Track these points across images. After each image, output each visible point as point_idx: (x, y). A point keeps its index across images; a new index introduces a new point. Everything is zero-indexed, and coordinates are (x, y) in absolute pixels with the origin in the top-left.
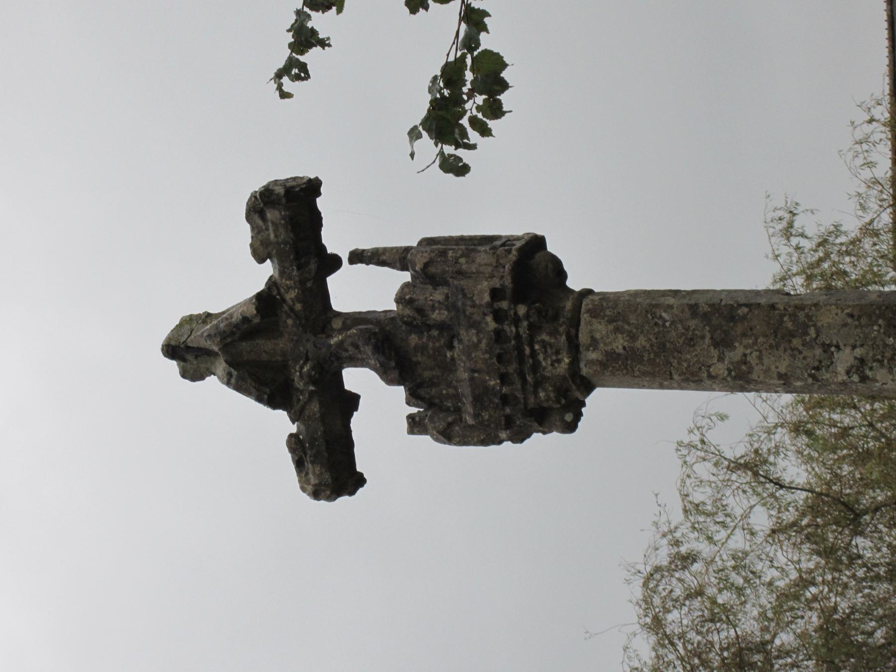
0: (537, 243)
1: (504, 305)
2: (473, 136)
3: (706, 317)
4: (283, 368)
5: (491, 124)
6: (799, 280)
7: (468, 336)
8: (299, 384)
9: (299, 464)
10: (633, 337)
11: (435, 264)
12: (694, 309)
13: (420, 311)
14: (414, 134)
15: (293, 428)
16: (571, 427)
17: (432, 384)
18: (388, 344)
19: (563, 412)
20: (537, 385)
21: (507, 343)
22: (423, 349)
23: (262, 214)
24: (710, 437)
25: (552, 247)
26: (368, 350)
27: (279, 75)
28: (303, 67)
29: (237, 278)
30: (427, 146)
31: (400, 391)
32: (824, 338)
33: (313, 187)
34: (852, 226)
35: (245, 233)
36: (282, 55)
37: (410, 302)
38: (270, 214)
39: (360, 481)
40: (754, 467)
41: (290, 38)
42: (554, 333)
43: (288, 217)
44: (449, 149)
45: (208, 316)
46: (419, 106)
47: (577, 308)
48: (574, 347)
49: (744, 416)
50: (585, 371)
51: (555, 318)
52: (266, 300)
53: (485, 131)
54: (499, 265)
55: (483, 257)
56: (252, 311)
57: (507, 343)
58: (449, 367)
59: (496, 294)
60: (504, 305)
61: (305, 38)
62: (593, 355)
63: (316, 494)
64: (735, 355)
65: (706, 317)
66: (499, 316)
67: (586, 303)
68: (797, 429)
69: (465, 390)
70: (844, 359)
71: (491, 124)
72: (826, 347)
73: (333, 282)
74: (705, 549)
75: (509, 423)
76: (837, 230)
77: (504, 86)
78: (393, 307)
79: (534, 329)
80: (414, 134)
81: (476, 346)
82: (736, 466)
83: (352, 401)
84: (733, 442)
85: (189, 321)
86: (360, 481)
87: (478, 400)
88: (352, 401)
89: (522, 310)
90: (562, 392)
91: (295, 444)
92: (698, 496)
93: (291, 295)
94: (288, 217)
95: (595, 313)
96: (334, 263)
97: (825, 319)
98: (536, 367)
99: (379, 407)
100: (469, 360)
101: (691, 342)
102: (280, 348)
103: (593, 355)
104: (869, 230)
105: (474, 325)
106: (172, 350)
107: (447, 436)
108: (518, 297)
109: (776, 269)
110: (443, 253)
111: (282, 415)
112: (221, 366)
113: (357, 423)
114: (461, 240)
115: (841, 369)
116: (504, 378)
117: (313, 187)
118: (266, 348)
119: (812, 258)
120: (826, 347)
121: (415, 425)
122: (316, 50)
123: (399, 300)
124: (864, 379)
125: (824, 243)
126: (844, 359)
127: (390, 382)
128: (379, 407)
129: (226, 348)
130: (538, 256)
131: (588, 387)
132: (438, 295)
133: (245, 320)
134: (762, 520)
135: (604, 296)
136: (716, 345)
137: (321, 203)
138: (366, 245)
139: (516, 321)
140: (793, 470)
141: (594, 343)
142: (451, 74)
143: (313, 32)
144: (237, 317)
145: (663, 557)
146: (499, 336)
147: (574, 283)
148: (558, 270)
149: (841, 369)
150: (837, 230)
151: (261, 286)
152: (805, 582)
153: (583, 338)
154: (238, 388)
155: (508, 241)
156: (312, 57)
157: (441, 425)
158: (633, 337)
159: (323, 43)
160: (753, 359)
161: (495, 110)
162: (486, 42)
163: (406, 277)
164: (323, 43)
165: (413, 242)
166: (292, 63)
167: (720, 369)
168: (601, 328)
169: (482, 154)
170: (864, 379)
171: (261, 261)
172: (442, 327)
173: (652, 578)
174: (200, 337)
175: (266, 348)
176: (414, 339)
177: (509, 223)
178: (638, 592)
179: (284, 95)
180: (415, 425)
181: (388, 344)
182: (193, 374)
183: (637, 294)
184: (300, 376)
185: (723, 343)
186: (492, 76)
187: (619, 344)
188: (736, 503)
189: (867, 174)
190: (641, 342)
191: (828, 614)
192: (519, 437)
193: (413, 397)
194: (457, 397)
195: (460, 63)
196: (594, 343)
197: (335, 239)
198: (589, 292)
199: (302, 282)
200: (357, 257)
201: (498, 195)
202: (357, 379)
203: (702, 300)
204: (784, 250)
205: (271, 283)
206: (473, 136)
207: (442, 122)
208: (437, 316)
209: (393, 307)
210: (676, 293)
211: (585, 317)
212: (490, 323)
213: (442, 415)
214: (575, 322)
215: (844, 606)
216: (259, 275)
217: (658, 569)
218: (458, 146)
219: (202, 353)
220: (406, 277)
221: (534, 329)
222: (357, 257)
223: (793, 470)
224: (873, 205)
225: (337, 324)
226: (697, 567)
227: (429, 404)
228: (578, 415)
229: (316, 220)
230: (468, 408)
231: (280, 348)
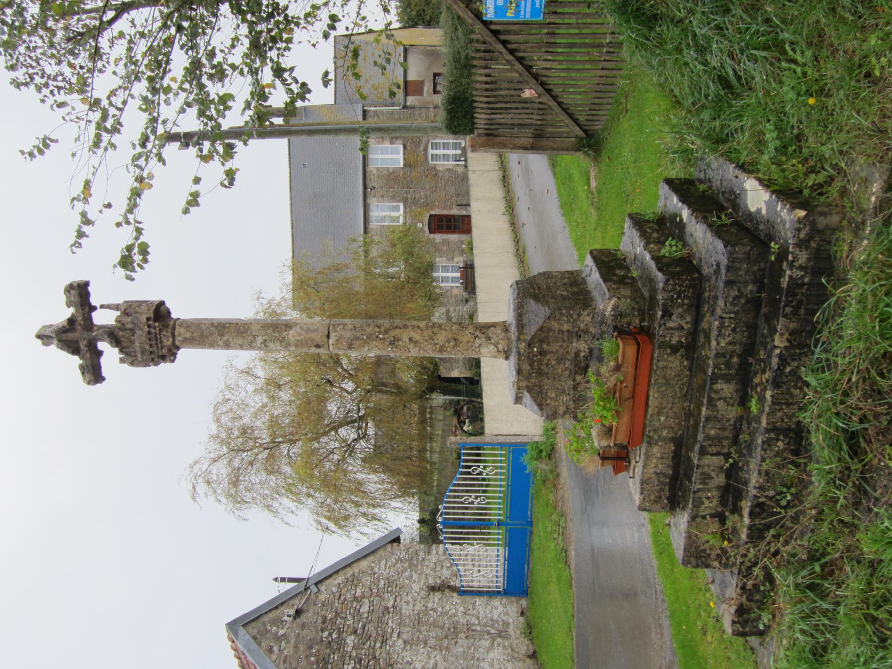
0: (162, 303)
1: (151, 322)
2: (137, 268)
3: (216, 327)
4: (77, 342)
5: (144, 265)
6: (262, 314)
7: (139, 332)
8: (82, 347)
9: (83, 373)
10: (193, 333)
11: (128, 309)
12: (212, 324)
13: (123, 324)
14: (115, 266)
15: (81, 362)
16: (173, 361)
17: (127, 347)
18: (114, 336)
19: (170, 355)
20: (162, 348)
21: (153, 334)
22: (124, 337)
23: (69, 292)
24: (233, 363)
25: (167, 304)
26: (106, 337)
27: (72, 246)
28: (80, 244)
29: (61, 312)
30: (121, 271)
31: (117, 350)
32: (253, 334)
33: (87, 284)
34: (278, 298)
35: (64, 298)
36: (73, 239)
37: (120, 321)
38: (73, 292)
39: (103, 379)
40: (248, 372)
41: (76, 234)
42: (167, 332)
43: (80, 294)
44: (129, 273)
45: (51, 325)
46: (118, 258)
47: (175, 324)
48: (174, 336)
49: (244, 357)
50: (177, 344)
51: (168, 327)
52: (71, 321)
53: (142, 268)
54: (149, 310)
55: (144, 307)
56: (66, 324)
57: (153, 334)
58: (133, 342)
59: (148, 319)
60: (151, 322)
61: (81, 235)
62: (180, 339)
63: (89, 383)
64: (225, 339)
65: (216, 327)
66: (149, 326)
67: (178, 322)
68: (261, 359)
69: (138, 349)
70: (260, 340)
71: (144, 265)
72: (254, 336)
73: (94, 315)
74: (233, 398)
75: (153, 360)
76: (273, 299)
77: (148, 253)
78: (114, 323)
79: (160, 330)
80: (115, 266)
81: (141, 336)
82: (242, 372)
83: (100, 353)
84: (242, 366)
85: (45, 327)
86: (103, 379)
87: (142, 353)
88: (100, 353)
89: (157, 324)
90: (170, 350)
91: (82, 367)
92: (229, 382)
93: (80, 319)
94: (80, 294)
95: (181, 325)
96: (95, 308)
97: (253, 328)
98: (161, 342)
99: (110, 355)
100: (140, 339)
101: (211, 335)
102: (78, 336)
103: (180, 339)
104: (283, 299)
105: (141, 329)
106: (39, 336)
107: (132, 364)
108: (155, 320)
109: (254, 310)
110: (131, 306)
111: (76, 358)
112: (55, 341)
113: (103, 360)
114: (137, 302)
115: (258, 343)
116: (151, 346)
117: (87, 284)
118: (71, 336)
119: (265, 307)
120: (254, 336)
121: (122, 361)
122: (85, 239)
123: (116, 321)
124: (266, 346)
125: (269, 302)
126: (260, 340)
127: (113, 347)
128: (110, 355)
129: (57, 335)
130: (162, 307)
131: (178, 348)
132: (129, 319)
133: (64, 327)
134: (250, 388)
135: (184, 320)
136: (219, 335)
137: (90, 289)
138: (105, 303)
139: (155, 328)
140: (260, 373)
141: (180, 335)
142: (129, 248)
143: (84, 233)
144: (61, 326)
145: (220, 399)
146: (149, 333)
147: (174, 315)
148: (169, 312)
149: (258, 343)
150: (273, 299)
151: (69, 316)
152: (264, 406)
153: (177, 333)
154: (61, 349)
155: (152, 303)
156: (83, 241)
157: (130, 361)
158: (193, 333)
159: (87, 236)
160: (231, 340)
161: (145, 261)
162: (142, 239)
163: (119, 313)
164: (87, 236)
165: (121, 302)
166: (76, 242)
167: (221, 343)
168: (182, 330)
169: (138, 274)
170: (266, 346)
171: (69, 307)
172: (131, 329)
173: (216, 406)
174: (48, 332)
175: (71, 336)
176: (121, 333)
177: (153, 296)
178: (212, 410)
179: (73, 253)
180: (122, 361)
181: (114, 336)
182: (46, 344)
183: (194, 319)
184: (83, 345)
185: (221, 335)
186: (144, 251)
187: (188, 335)
188: (242, 384)
189: (283, 282)
190: (195, 335)
191: (271, 416)
192: (156, 364)
193: (121, 351)
194: (135, 352)
195: (133, 245)
196: (180, 335)
197: (94, 301)
198: (179, 319)
199: (83, 314)
200: (102, 307)
201: (146, 288)
202: (102, 346)
203: (215, 322)
204: (257, 304)
205: (73, 315)
206: (137, 268)
207: (126, 262)
208: (129, 326)
209: (114, 323)
210: (207, 319)
211: (177, 327)
212: (146, 329)
213: (130, 357)
214: (174, 328)
215: (276, 413)
216: (70, 312)
217: (218, 403)
218: (131, 271)
219: (49, 337)
220: (119, 313)
221: (160, 330)
222: (102, 307)
223: (260, 373)
224: (285, 291)
225: (95, 328)
226: (231, 402)
227: (127, 354)
228: (175, 358)
229: (88, 294)
230: (139, 355)
231: (78, 336)
